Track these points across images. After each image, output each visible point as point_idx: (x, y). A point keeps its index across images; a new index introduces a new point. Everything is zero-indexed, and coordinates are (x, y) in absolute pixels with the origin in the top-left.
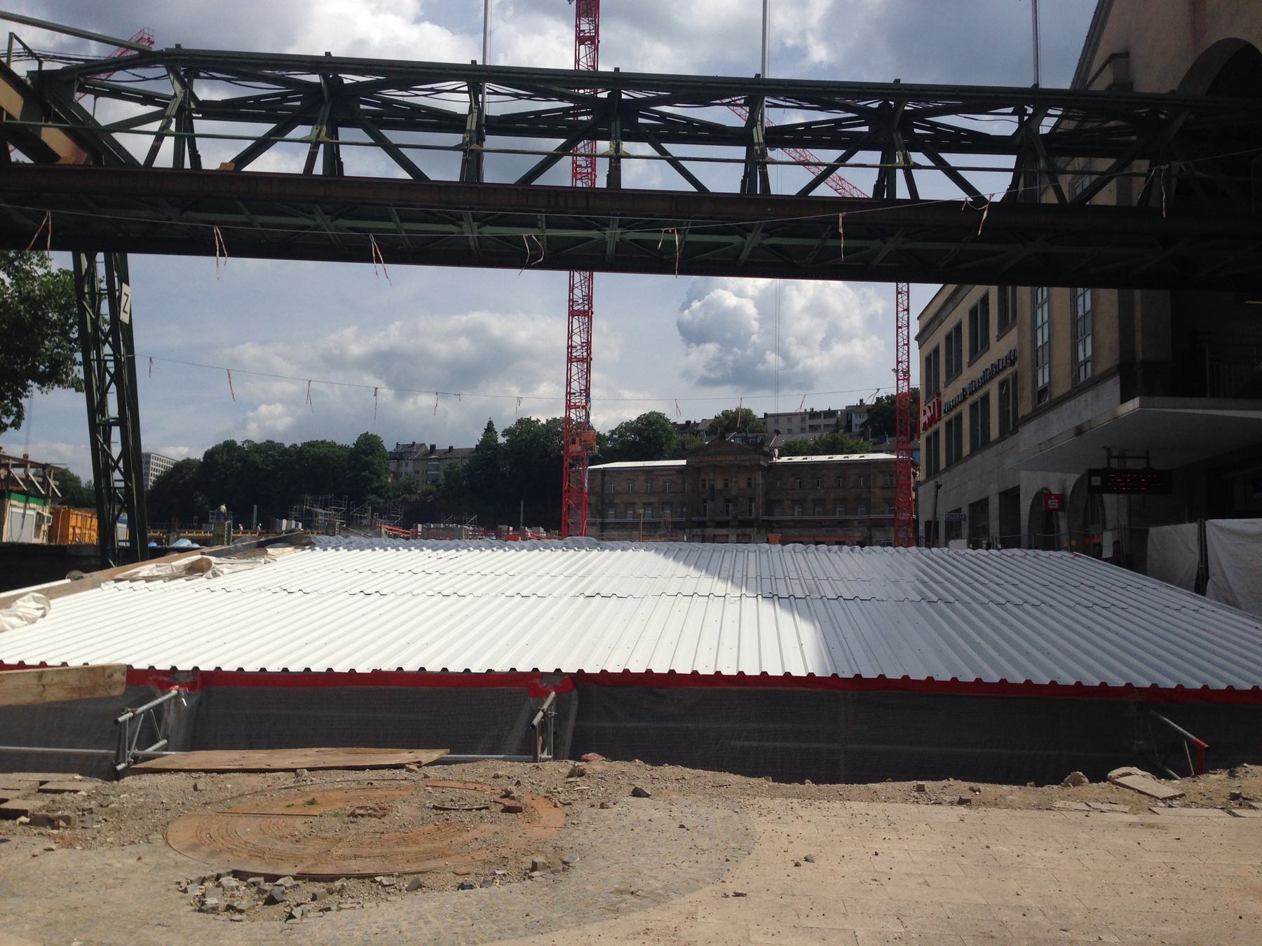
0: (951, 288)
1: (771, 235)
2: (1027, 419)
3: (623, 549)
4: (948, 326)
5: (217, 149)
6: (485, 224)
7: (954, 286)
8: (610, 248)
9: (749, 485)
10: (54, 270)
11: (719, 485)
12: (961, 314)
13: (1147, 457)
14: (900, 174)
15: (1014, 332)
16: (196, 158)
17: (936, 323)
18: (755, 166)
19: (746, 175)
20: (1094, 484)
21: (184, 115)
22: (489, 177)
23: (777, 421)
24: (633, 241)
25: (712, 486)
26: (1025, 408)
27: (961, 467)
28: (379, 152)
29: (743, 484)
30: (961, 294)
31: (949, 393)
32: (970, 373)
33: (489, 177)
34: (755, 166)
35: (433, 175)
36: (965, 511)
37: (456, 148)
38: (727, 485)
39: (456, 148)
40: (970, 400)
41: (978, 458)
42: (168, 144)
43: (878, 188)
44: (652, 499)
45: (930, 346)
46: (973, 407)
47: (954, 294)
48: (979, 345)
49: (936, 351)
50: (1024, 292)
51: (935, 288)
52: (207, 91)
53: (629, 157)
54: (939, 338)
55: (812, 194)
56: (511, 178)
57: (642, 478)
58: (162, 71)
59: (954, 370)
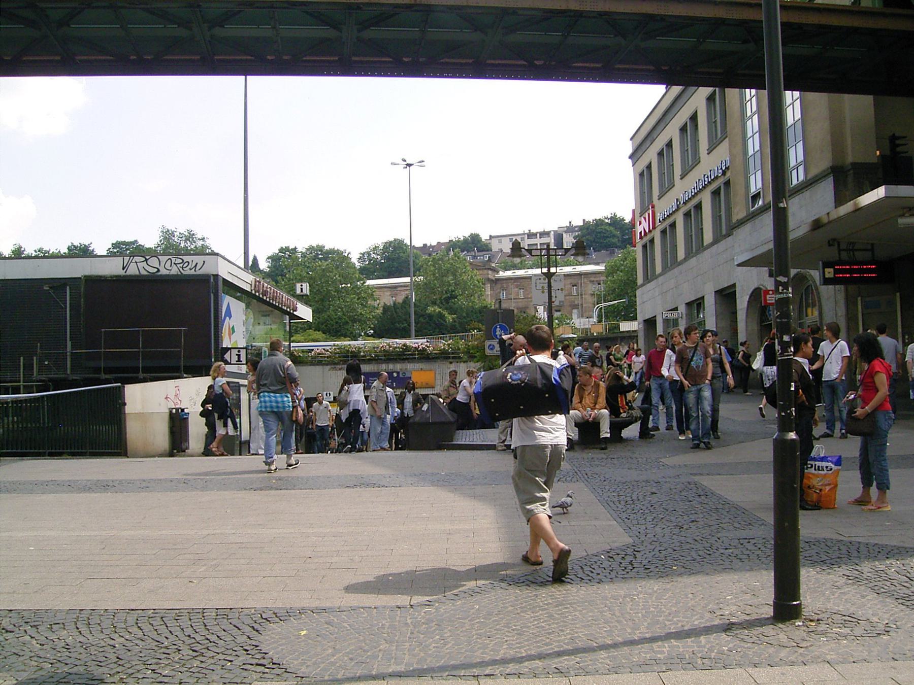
0: (676, 89)
2: (741, 223)
3: (82, 252)
4: (660, 143)
7: (680, 88)
10: (560, 419)
13: (872, 250)
15: (725, 145)
17: (648, 142)
20: (827, 276)
23: (500, 242)
26: (739, 213)
27: (676, 271)
30: (684, 98)
31: (664, 207)
32: (683, 188)
36: (682, 309)
40: (684, 209)
41: (693, 261)
45: (642, 164)
46: (687, 215)
47: (683, 91)
48: (691, 162)
49: (649, 167)
51: (658, 90)
54: (651, 155)
57: (388, 293)
59: (667, 187)
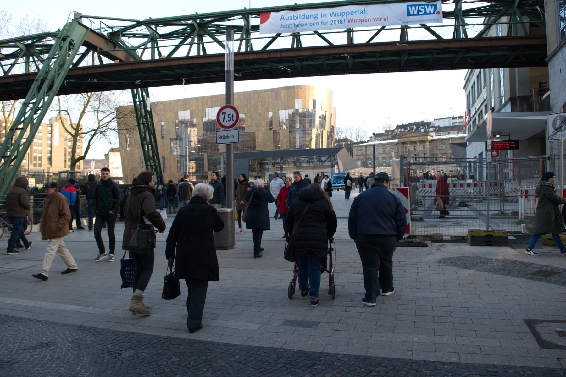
0: (470, 70)
1: (411, 56)
4: (471, 84)
5: (166, 48)
6: (250, 65)
8: (350, 65)
9: (424, 148)
11: (412, 149)
12: (474, 78)
14: (156, 49)
16: (204, 50)
18: (460, 26)
19: (455, 30)
21: (153, 38)
22: (356, 41)
24: (358, 62)
25: (409, 150)
28: (216, 44)
29: (422, 148)
33: (356, 41)
34: (460, 26)
35: (335, 43)
37: (344, 32)
38: (424, 148)
39: (344, 32)
42: (195, 47)
43: (456, 31)
44: (386, 156)
50: (487, 70)
52: (162, 30)
53: (468, 25)
54: (469, 88)
55: (371, 42)
56: (364, 41)
58: (240, 16)
